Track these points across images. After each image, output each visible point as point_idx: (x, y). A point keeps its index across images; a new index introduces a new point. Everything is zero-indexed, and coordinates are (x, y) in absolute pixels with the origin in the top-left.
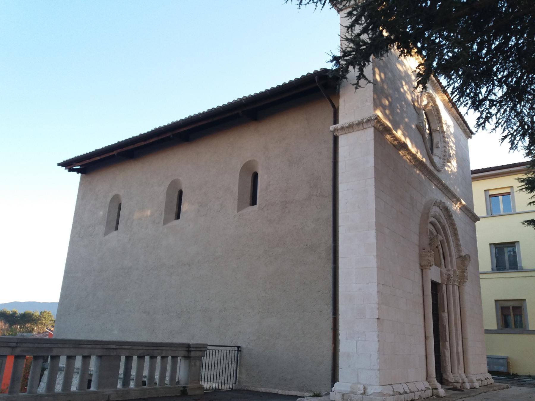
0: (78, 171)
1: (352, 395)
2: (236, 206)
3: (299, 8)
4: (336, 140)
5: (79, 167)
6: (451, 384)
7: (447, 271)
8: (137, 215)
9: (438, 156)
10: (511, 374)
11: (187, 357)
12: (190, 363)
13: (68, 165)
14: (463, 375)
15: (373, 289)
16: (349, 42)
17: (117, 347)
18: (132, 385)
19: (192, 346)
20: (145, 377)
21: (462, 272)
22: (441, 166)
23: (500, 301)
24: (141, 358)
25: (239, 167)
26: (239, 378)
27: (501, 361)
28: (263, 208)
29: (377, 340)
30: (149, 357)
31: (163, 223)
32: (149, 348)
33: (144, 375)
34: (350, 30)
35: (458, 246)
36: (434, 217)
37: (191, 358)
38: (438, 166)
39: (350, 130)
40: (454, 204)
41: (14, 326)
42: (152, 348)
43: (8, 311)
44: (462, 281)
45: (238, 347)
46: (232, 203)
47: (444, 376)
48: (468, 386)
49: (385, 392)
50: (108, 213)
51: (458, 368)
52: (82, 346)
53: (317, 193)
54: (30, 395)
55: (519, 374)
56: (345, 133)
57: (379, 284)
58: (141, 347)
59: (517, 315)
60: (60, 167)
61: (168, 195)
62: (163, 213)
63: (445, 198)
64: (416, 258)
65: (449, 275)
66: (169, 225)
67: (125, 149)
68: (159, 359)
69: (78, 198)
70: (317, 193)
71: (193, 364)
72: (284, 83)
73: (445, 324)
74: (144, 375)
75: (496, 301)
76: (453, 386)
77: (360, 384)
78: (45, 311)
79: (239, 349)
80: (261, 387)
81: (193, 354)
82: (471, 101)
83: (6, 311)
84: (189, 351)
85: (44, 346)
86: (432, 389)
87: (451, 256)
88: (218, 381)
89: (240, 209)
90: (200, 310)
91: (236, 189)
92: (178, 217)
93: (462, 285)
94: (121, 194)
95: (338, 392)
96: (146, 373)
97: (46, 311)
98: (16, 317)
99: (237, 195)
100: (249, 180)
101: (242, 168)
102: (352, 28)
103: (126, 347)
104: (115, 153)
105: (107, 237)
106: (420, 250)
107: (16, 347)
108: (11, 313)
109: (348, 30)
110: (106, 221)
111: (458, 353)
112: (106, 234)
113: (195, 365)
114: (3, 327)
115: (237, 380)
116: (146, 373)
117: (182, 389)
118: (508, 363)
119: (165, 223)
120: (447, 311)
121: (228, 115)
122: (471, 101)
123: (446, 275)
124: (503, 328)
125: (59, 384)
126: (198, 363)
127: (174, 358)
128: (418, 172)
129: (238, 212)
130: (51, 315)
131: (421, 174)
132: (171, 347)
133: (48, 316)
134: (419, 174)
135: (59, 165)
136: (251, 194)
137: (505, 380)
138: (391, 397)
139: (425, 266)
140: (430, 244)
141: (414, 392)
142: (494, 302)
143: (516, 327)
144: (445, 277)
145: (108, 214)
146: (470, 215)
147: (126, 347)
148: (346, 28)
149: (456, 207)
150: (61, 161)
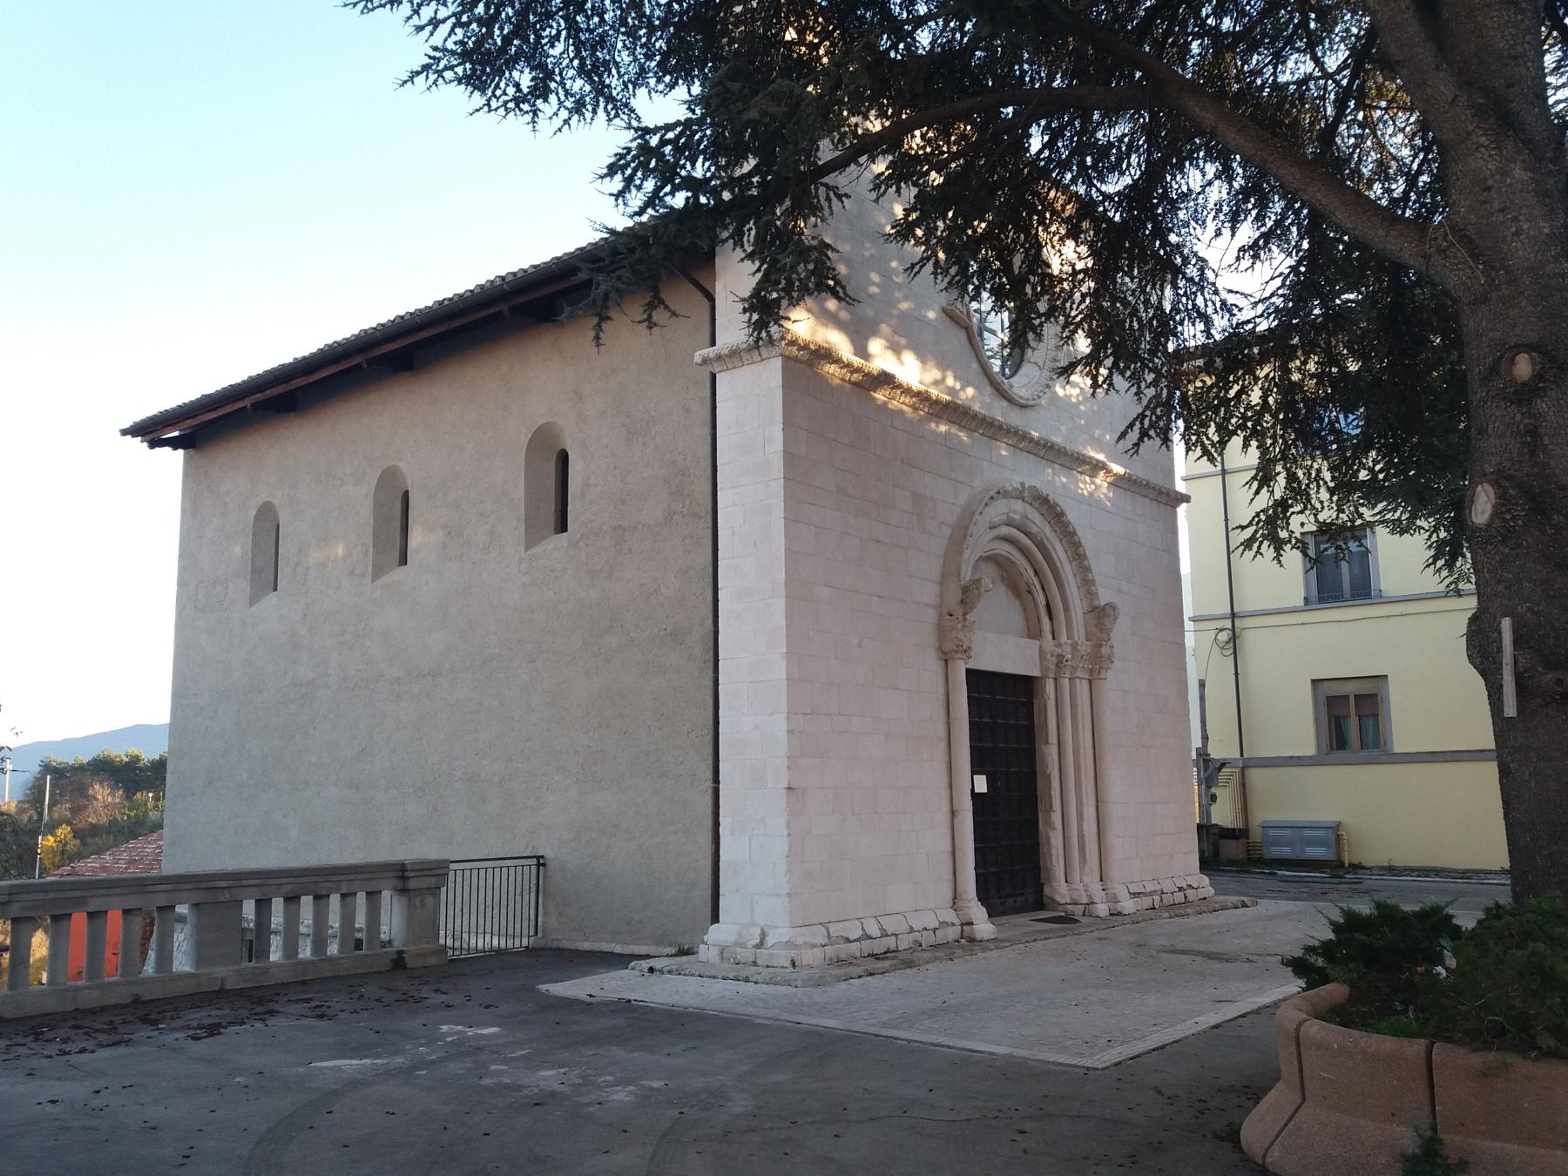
0: (174, 444)
1: (738, 949)
2: (522, 536)
3: (534, 131)
4: (714, 377)
5: (176, 434)
6: (1060, 908)
7: (1056, 646)
8: (315, 556)
9: (1035, 363)
10: (1347, 865)
11: (403, 891)
12: (410, 901)
13: (151, 431)
14: (1096, 887)
15: (780, 725)
18: (333, 949)
19: (409, 868)
20: (360, 930)
21: (1096, 646)
22: (1041, 389)
23: (1325, 683)
24: (292, 900)
25: (524, 440)
26: (544, 922)
27: (1322, 833)
28: (578, 542)
29: (786, 833)
30: (310, 898)
31: (373, 577)
32: (305, 879)
33: (357, 926)
34: (621, 199)
35: (1087, 583)
36: (1007, 525)
37: (411, 893)
38: (1022, 394)
39: (737, 362)
40: (1088, 479)
41: (138, 795)
42: (314, 879)
43: (116, 757)
44: (1097, 667)
45: (538, 858)
46: (513, 527)
47: (1047, 890)
48: (1102, 909)
49: (800, 941)
50: (253, 548)
51: (1082, 870)
53: (684, 506)
54: (52, 988)
55: (1364, 864)
56: (728, 369)
57: (791, 714)
58: (287, 880)
59: (1368, 716)
60: (129, 436)
61: (378, 506)
62: (371, 550)
63: (1050, 471)
64: (928, 636)
65: (1060, 657)
66: (385, 579)
67: (268, 393)
68: (335, 900)
69: (184, 511)
70: (684, 506)
71: (418, 903)
73: (1048, 772)
74: (357, 926)
75: (1314, 682)
76: (1066, 912)
77: (754, 924)
79: (541, 862)
80: (585, 940)
81: (413, 884)
84: (404, 878)
85: (68, 894)
86: (962, 925)
87: (1066, 609)
88: (503, 931)
89: (532, 540)
90: (462, 779)
91: (519, 493)
92: (403, 561)
93: (1096, 676)
94: (276, 502)
95: (714, 945)
96: (361, 921)
98: (140, 769)
99: (522, 508)
100: (551, 468)
101: (529, 442)
102: (623, 197)
103: (252, 882)
104: (247, 403)
105: (254, 608)
106: (940, 616)
107: (9, 902)
108: (126, 759)
109: (616, 200)
110: (249, 570)
111: (1081, 837)
112: (253, 601)
113: (423, 905)
114: (110, 799)
115: (539, 929)
116: (361, 921)
117: (395, 956)
118: (1338, 837)
119: (375, 577)
120: (1055, 741)
121: (482, 314)
123: (1052, 655)
124: (1332, 749)
126: (429, 900)
127: (373, 895)
128: (943, 428)
129: (526, 550)
131: (954, 430)
132: (362, 873)
134: (948, 433)
135: (124, 432)
136: (556, 504)
137: (1296, 882)
138: (815, 949)
139: (950, 652)
140: (962, 602)
141: (896, 935)
142: (1309, 684)
143: (1363, 746)
144: (1051, 663)
145: (252, 553)
146: (1152, 494)
147: (252, 882)
148: (613, 198)
149: (1093, 483)
150: (127, 424)
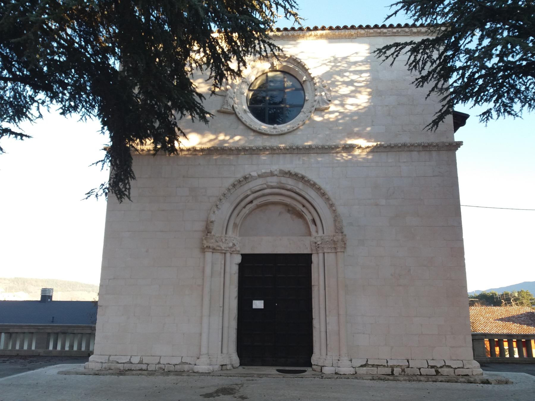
16: (94, 109)
17: (43, 328)
52: (23, 328)
72: (330, 42)
78: (521, 290)
82: (109, 162)
83: (486, 293)
97: (523, 290)
103: (48, 328)
122: (109, 162)
125: (506, 352)
130: (530, 294)
133: (527, 295)
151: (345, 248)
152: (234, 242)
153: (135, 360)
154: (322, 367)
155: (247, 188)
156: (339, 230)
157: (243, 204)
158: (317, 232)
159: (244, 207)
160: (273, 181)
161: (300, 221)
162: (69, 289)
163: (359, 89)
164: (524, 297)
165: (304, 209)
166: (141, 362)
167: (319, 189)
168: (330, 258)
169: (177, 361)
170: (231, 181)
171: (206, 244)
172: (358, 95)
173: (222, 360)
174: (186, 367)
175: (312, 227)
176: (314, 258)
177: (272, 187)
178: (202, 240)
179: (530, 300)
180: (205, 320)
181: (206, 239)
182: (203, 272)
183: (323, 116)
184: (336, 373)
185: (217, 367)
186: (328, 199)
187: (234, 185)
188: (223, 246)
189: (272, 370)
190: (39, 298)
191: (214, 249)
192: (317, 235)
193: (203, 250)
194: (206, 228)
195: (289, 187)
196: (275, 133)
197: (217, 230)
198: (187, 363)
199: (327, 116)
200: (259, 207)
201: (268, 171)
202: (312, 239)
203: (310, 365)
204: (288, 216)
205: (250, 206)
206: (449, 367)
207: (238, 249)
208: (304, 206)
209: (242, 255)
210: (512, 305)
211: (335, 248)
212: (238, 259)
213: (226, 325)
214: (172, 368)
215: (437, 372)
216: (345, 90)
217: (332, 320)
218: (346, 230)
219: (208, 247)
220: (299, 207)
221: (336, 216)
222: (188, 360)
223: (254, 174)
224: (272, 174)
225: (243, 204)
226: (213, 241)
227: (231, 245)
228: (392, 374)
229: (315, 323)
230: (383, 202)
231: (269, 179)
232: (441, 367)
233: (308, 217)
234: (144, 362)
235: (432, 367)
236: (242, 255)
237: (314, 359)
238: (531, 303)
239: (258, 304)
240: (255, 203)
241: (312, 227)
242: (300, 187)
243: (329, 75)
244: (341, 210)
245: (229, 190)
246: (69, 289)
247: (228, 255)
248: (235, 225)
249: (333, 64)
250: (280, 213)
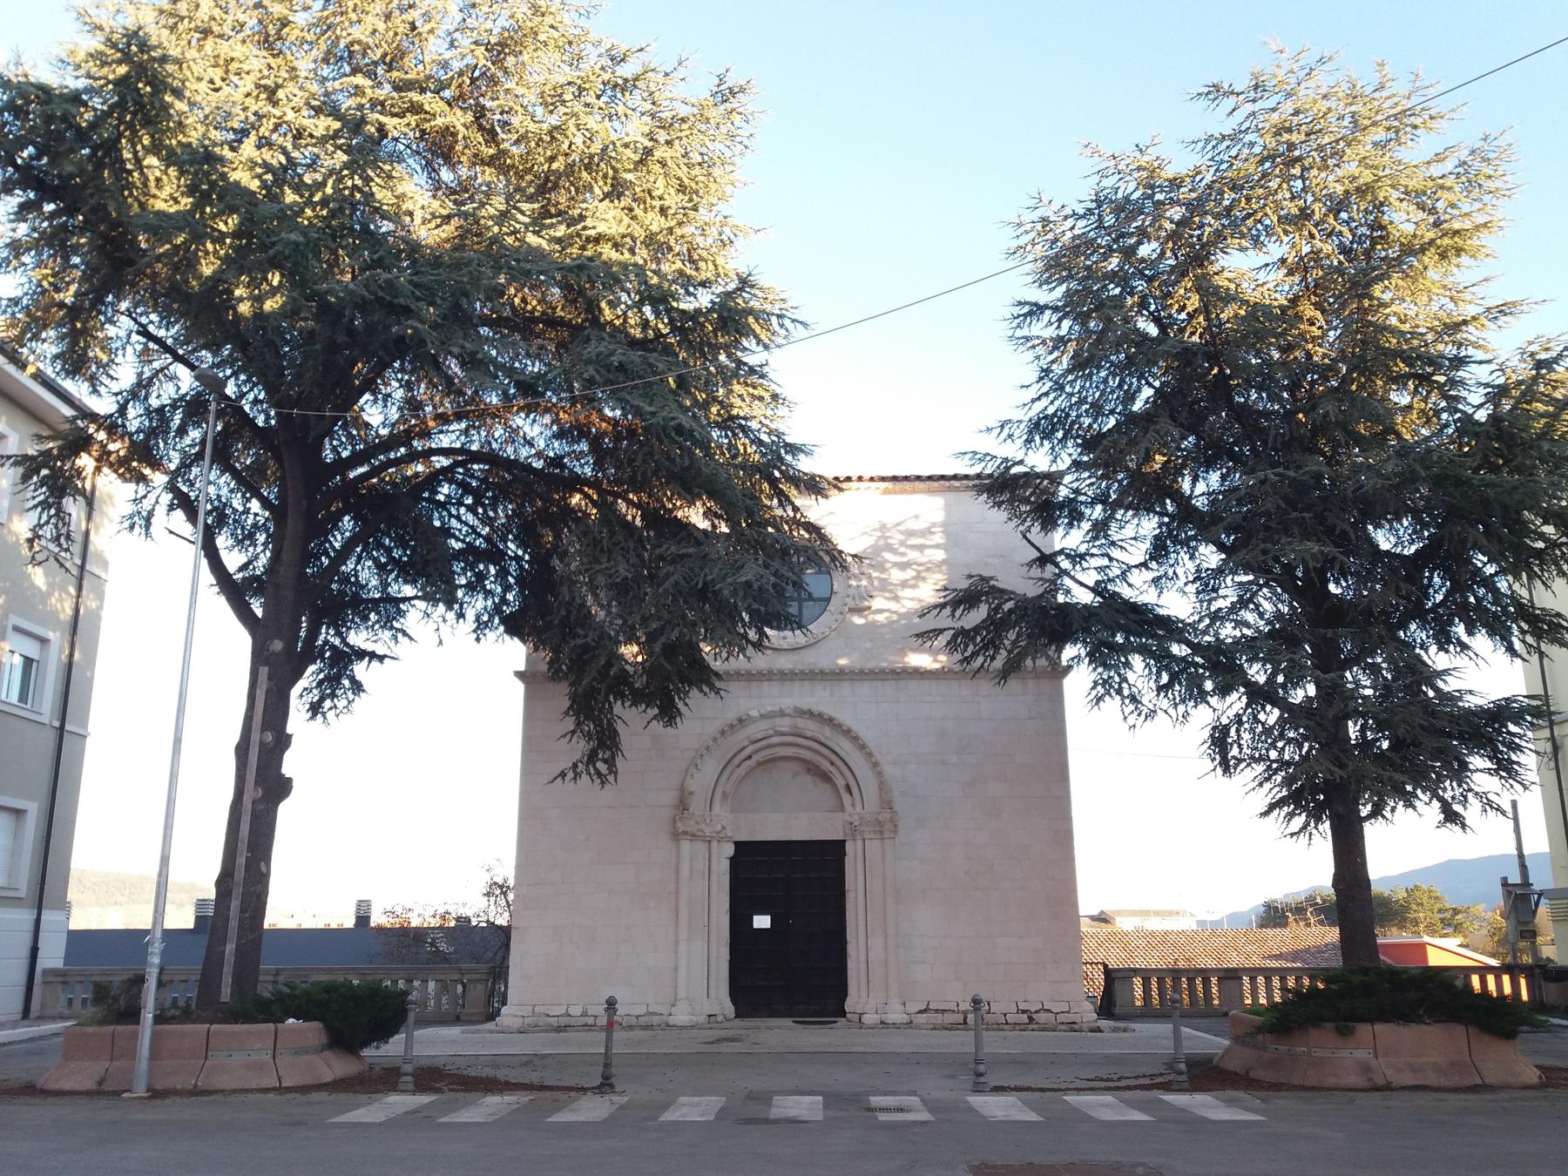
151: (896, 832)
152: (723, 823)
153: (576, 1011)
154: (861, 1014)
155: (742, 736)
156: (887, 804)
157: (737, 761)
158: (853, 805)
159: (738, 766)
160: (784, 724)
161: (827, 786)
162: (120, 899)
163: (923, 574)
164: (1421, 904)
165: (832, 769)
166: (584, 1014)
167: (856, 738)
168: (874, 847)
169: (641, 1010)
170: (718, 724)
171: (681, 827)
172: (921, 584)
173: (708, 1007)
174: (655, 1020)
175: (846, 797)
176: (849, 847)
177: (783, 734)
178: (675, 821)
179: (1440, 911)
180: (683, 948)
181: (681, 820)
182: (677, 872)
183: (865, 617)
184: (882, 1023)
185: (702, 1019)
186: (870, 755)
187: (723, 733)
188: (708, 831)
189: (788, 1022)
190: (191, 925)
191: (693, 835)
192: (854, 811)
193: (676, 836)
194: (681, 802)
195: (809, 734)
196: (785, 647)
197: (697, 806)
198: (656, 1014)
199: (871, 617)
200: (760, 764)
201: (777, 708)
202: (846, 817)
203: (843, 1014)
204: (808, 779)
205: (748, 763)
206: (1049, 1011)
207: (730, 834)
208: (832, 764)
209: (735, 843)
210: (1308, 925)
211: (881, 832)
212: (730, 850)
213: (714, 953)
214: (634, 1021)
215: (1030, 1018)
216: (896, 575)
217: (876, 943)
218: (897, 806)
219: (686, 833)
220: (826, 765)
221: (882, 783)
222: (658, 1009)
223: (754, 713)
224: (782, 714)
225: (737, 761)
226: (692, 822)
227: (719, 827)
228: (965, 1023)
229: (851, 949)
230: (954, 759)
231: (777, 721)
232: (1037, 1012)
233: (840, 782)
234: (590, 1013)
235: (1024, 1012)
236: (735, 843)
237: (849, 1005)
238: (1442, 920)
239: (762, 922)
240: (755, 758)
241: (846, 797)
242: (825, 733)
243: (877, 550)
244: (889, 771)
245: (715, 739)
246: (120, 899)
247: (714, 844)
248: (725, 796)
249: (879, 534)
250: (795, 775)
